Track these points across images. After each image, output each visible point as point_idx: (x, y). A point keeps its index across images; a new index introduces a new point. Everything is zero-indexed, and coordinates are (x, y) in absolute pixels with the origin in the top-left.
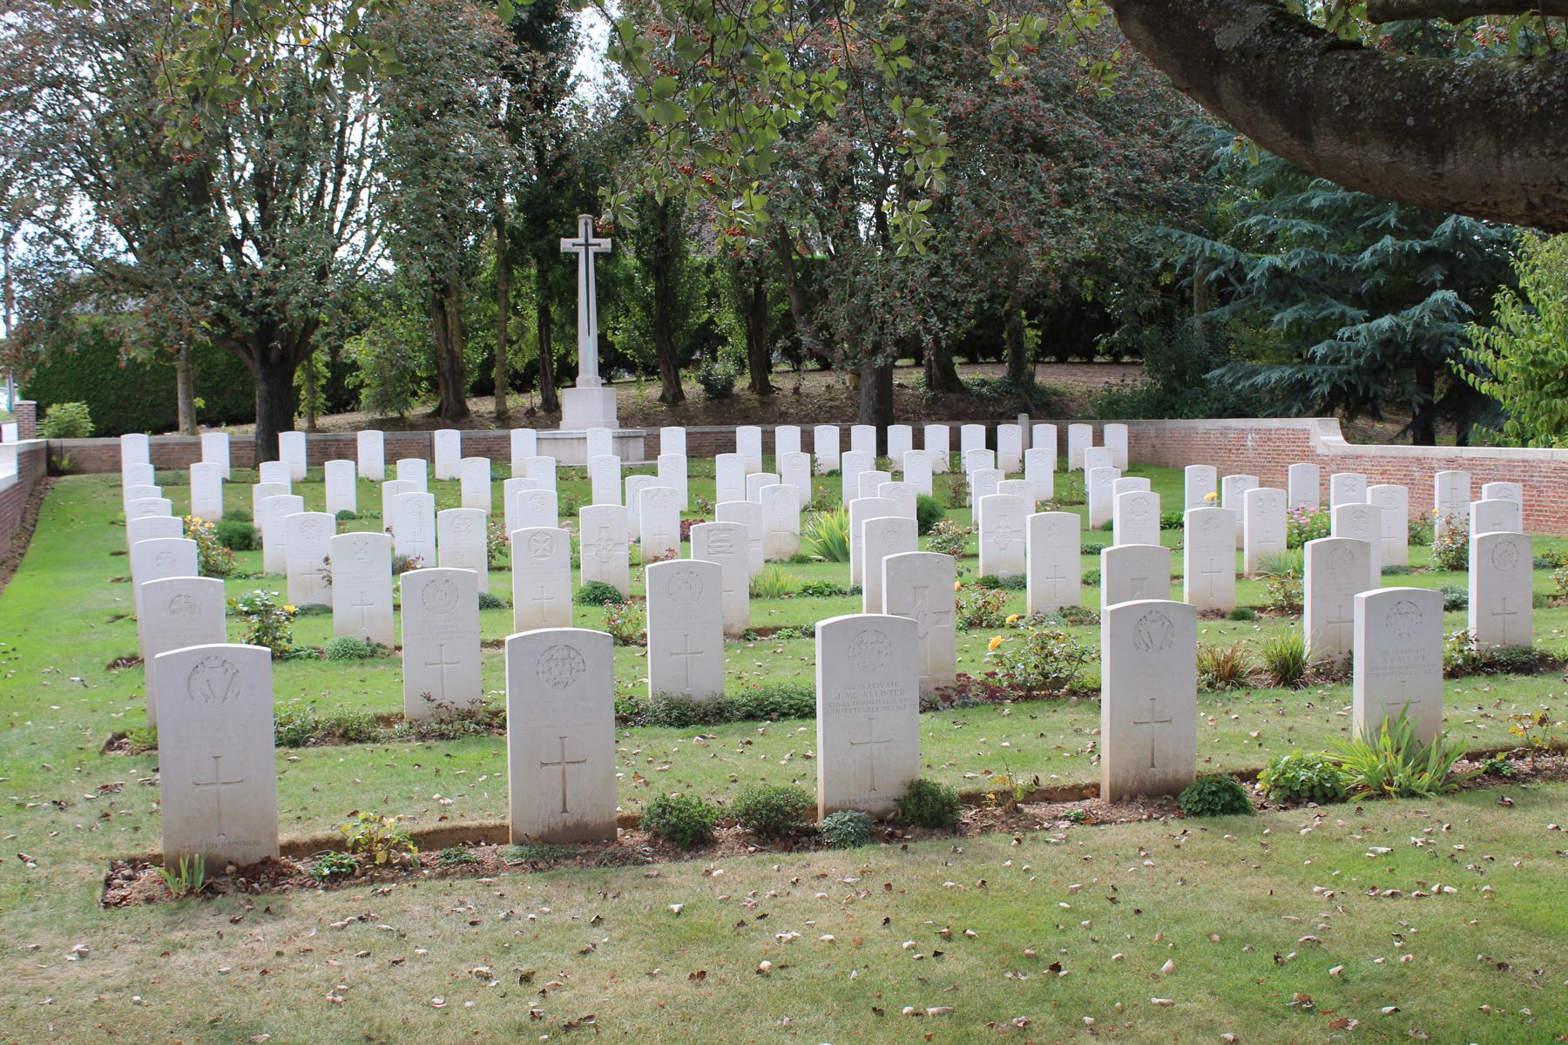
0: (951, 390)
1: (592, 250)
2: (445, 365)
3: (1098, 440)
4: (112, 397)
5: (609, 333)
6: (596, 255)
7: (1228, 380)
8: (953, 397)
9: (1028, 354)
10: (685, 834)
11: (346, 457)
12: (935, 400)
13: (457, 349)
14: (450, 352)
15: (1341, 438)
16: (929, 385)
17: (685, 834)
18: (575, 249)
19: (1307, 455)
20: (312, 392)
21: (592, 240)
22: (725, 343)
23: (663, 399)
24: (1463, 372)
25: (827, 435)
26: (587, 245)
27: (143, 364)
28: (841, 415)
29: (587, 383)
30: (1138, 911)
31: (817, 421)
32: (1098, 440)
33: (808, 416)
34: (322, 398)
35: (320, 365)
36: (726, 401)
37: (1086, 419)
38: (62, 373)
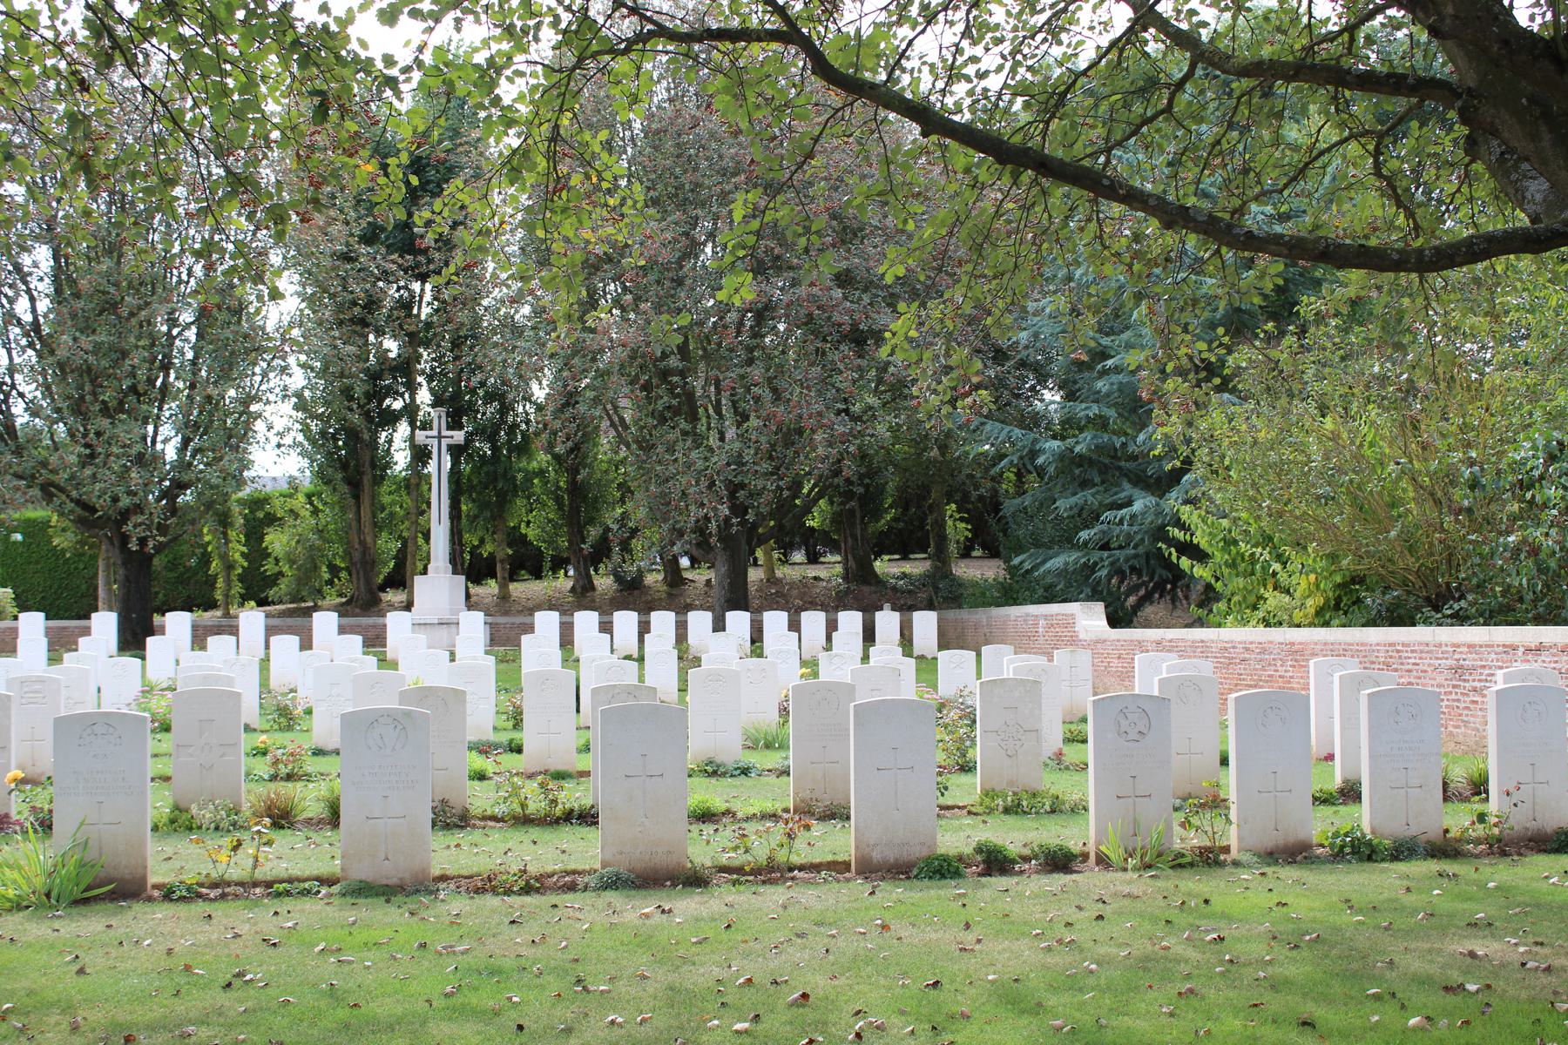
0: (866, 582)
1: (444, 442)
2: (357, 556)
3: (719, 626)
4: (84, 587)
5: (523, 525)
6: (450, 448)
7: (1027, 566)
8: (866, 589)
9: (953, 547)
10: (995, 863)
11: (231, 634)
12: (848, 592)
13: (369, 540)
14: (362, 543)
15: (1105, 622)
16: (846, 578)
17: (995, 863)
18: (428, 441)
19: (1073, 641)
20: (228, 582)
21: (445, 433)
22: (540, 530)
23: (573, 590)
24: (1174, 554)
25: (814, 621)
26: (440, 437)
27: (63, 551)
28: (833, 604)
29: (437, 570)
30: (520, 1027)
31: (837, 609)
32: (719, 626)
33: (795, 601)
34: (237, 588)
35: (237, 556)
36: (636, 592)
37: (823, 607)
38: (37, 562)
